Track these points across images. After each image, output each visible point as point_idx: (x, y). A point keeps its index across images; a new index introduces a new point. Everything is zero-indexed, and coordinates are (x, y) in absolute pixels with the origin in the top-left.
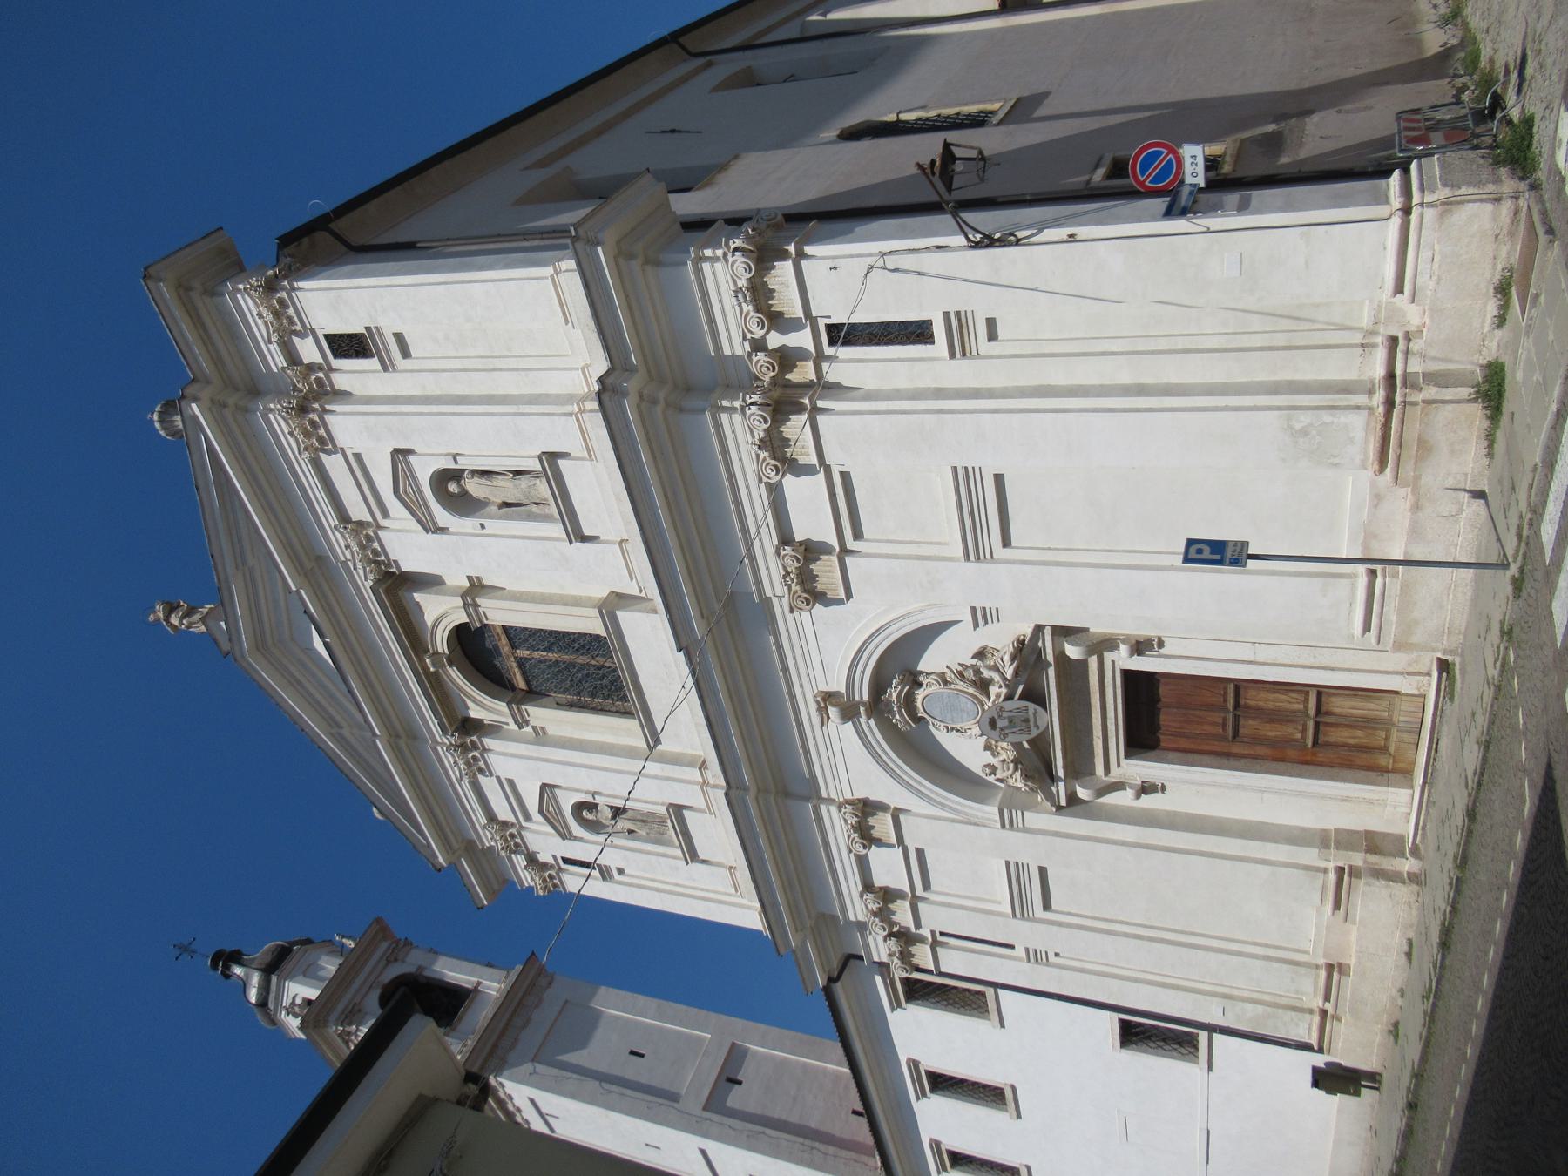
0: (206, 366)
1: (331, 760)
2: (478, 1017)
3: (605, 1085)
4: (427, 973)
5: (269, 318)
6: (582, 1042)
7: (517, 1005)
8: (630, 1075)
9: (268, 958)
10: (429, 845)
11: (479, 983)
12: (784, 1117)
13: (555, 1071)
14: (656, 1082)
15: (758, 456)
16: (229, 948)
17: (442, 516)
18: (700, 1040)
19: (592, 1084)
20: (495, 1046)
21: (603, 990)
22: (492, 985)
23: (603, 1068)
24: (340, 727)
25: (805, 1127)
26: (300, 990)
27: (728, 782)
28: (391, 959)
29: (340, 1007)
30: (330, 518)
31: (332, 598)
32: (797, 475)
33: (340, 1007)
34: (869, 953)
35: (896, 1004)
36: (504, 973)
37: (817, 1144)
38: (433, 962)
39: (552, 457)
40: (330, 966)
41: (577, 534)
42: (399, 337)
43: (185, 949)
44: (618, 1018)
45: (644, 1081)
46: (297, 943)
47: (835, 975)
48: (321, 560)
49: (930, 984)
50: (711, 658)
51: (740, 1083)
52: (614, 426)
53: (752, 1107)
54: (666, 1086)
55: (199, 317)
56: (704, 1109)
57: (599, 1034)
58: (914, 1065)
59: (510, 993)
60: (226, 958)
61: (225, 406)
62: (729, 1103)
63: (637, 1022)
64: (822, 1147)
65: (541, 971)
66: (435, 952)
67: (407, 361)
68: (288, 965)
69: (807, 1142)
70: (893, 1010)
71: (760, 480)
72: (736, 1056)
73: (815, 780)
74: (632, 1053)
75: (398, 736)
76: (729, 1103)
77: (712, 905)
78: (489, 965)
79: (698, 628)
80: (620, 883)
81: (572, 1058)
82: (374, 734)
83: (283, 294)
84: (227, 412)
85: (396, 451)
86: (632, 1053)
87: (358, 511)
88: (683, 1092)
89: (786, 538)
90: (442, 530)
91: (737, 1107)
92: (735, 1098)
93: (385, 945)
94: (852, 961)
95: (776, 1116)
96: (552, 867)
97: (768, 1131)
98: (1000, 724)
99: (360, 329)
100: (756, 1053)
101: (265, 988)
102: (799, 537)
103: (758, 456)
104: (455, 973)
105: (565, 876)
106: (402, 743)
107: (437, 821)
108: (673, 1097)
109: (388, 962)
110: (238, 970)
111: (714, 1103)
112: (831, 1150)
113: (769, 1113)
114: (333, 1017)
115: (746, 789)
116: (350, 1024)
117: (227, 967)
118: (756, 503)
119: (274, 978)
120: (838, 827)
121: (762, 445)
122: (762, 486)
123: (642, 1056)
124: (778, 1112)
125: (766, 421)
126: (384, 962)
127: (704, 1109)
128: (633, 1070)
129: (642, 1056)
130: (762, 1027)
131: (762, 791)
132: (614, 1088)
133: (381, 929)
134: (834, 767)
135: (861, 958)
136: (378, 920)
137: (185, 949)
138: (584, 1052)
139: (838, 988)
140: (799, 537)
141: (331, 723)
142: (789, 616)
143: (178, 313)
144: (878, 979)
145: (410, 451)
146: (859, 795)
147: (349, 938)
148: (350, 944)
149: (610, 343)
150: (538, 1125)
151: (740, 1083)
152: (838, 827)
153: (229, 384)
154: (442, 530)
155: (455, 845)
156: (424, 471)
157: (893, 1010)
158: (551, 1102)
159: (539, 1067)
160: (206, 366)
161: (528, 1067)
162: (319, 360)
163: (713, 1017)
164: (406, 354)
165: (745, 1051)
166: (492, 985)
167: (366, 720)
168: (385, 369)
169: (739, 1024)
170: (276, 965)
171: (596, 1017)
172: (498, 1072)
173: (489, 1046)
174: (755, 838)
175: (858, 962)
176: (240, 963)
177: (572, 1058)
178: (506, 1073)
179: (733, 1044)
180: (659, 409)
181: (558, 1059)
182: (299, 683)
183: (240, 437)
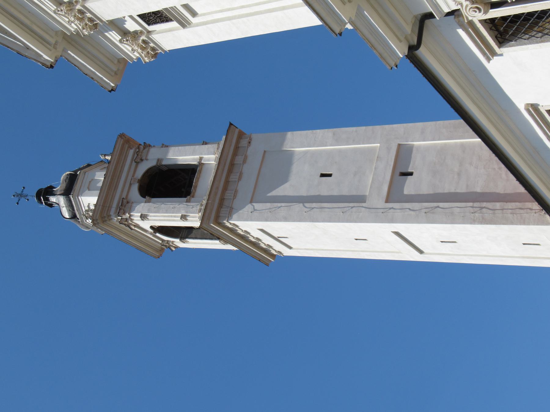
2: (204, 183)
3: (307, 205)
4: (164, 163)
5: (140, 51)
6: (284, 178)
7: (229, 165)
8: (325, 192)
9: (64, 185)
10: (28, 48)
11: (201, 159)
12: (453, 190)
13: (268, 205)
14: (345, 192)
16: (44, 186)
18: (373, 150)
19: (298, 207)
20: (222, 200)
21: (289, 134)
22: (207, 156)
23: (303, 193)
25: (419, 195)
26: (89, 201)
28: (138, 160)
29: (115, 205)
31: (392, 10)
33: (115, 205)
34: (436, 6)
35: (491, 53)
36: (216, 146)
37: (484, 204)
38: (167, 153)
40: (100, 176)
43: (20, 195)
44: (306, 152)
45: (335, 193)
46: (80, 169)
47: (415, 42)
49: (517, 17)
51: (411, 174)
53: (425, 190)
54: (354, 193)
56: (387, 201)
57: (295, 168)
58: (534, 108)
59: (220, 160)
60: (45, 193)
62: (406, 192)
63: (320, 152)
64: (490, 205)
65: (241, 135)
66: (165, 146)
68: (77, 187)
69: (477, 204)
70: (489, 60)
72: (403, 153)
74: (323, 175)
76: (406, 192)
77: (279, 14)
78: (205, 143)
80: (198, 25)
81: (279, 192)
83: (143, 37)
86: (323, 175)
88: (367, 194)
91: (413, 192)
92: (410, 186)
93: (131, 152)
94: (428, 22)
95: (446, 191)
96: (141, 32)
97: (441, 205)
100: (419, 147)
101: (70, 205)
104: (183, 156)
105: (155, 37)
107: (22, 23)
108: (360, 199)
109: (137, 163)
110: (53, 199)
111: (394, 195)
112: (498, 205)
113: (440, 191)
114: (112, 212)
116: (124, 214)
117: (47, 200)
119: (71, 196)
123: (330, 175)
124: (448, 188)
126: (134, 164)
127: (387, 201)
128: (326, 188)
129: (330, 175)
130: (420, 125)
132: (314, 205)
133: (125, 141)
135: (430, 16)
136: (122, 136)
137: (20, 195)
138: (287, 185)
139: (423, 53)
144: (461, 32)
147: (108, 155)
148: (109, 158)
150: (287, 252)
151: (411, 174)
155: (52, 41)
157: (489, 60)
158: (277, 228)
159: (257, 206)
161: (249, 207)
162: (138, 28)
163: (378, 128)
164: (194, 14)
165: (411, 148)
166: (207, 156)
168: (183, 26)
169: (400, 128)
170: (70, 188)
171: (291, 154)
172: (229, 217)
173: (217, 201)
175: (432, 20)
176: (53, 194)
177: (279, 192)
178: (235, 216)
179: (399, 145)
181: (268, 194)
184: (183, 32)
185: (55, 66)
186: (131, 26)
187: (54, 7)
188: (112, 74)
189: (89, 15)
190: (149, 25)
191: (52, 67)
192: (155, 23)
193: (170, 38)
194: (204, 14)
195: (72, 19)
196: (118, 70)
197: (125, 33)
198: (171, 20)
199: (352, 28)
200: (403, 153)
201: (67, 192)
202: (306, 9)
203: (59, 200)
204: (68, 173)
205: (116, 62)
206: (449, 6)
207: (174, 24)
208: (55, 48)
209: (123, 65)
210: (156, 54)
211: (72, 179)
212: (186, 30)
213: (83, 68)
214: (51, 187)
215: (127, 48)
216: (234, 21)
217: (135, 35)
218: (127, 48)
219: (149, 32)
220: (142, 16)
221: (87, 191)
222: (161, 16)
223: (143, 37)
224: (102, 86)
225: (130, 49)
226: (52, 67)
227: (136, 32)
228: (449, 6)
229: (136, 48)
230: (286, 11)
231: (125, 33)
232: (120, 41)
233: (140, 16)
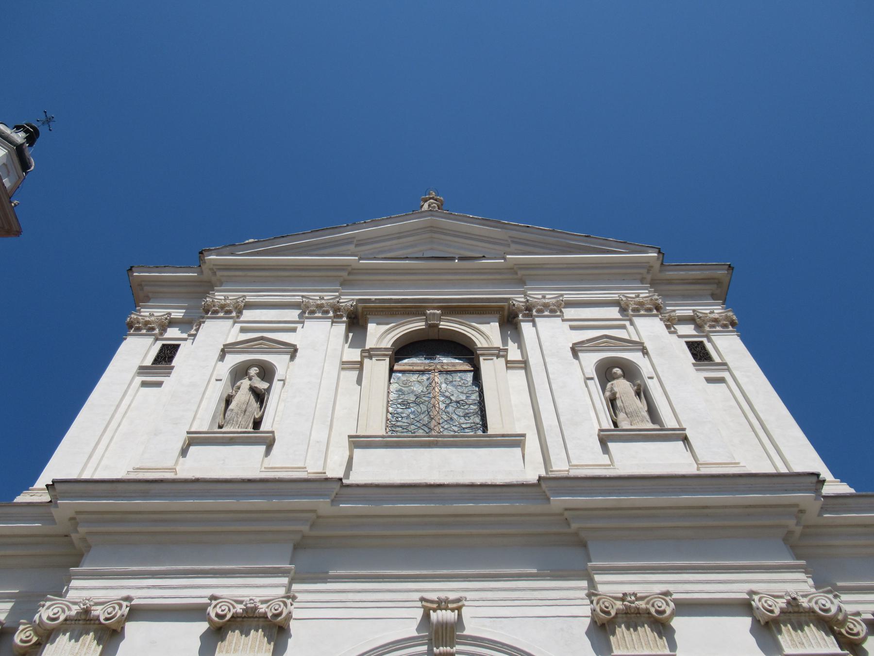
0: (671, 274)
1: (335, 229)
5: (147, 319)
10: (232, 254)
15: (241, 602)
16: (38, 141)
17: (233, 360)
24: (357, 245)
27: (348, 486)
30: (251, 298)
32: (203, 637)
39: (269, 443)
41: (194, 440)
42: (159, 384)
43: (48, 121)
48: (344, 283)
50: (519, 506)
52: (498, 490)
55: (699, 284)
60: (32, 137)
61: (648, 272)
67: (140, 383)
71: (213, 598)
73: (324, 580)
75: (349, 274)
82: (360, 259)
83: (157, 331)
84: (644, 271)
85: (296, 350)
87: (247, 315)
89: (137, 613)
90: (222, 358)
96: (161, 334)
99: (174, 363)
102: (131, 628)
103: (241, 602)
105: (151, 340)
106: (344, 274)
115: (335, 501)
117: (26, 131)
118: (733, 586)
120: (261, 591)
121: (793, 602)
122: (207, 601)
125: (107, 619)
131: (316, 520)
134: (343, 605)
136: (18, 233)
140: (131, 628)
141: (348, 241)
142: (417, 596)
143: (707, 274)
145: (293, 358)
146: (293, 624)
149: (841, 501)
152: (261, 591)
153: (345, 280)
154: (222, 358)
155: (219, 273)
156: (279, 361)
160: (671, 274)
162: (166, 336)
164: (144, 384)
167: (375, 258)
168: (141, 368)
174: (261, 496)
180: (305, 528)
182: (399, 238)
183: (629, 271)
184: (136, 363)
185: (198, 255)
186: (173, 333)
187: (248, 299)
188: (142, 283)
189: (221, 314)
190: (164, 345)
191: (201, 253)
192: (161, 350)
193: (136, 351)
194: (138, 391)
195: (228, 302)
196: (142, 290)
197: (172, 323)
198: (153, 364)
199: (15, 501)
200: (592, 379)
201: (19, 150)
202: (74, 476)
203: (19, 137)
204: (32, 168)
205: (150, 295)
206: (76, 589)
207: (149, 362)
208: (211, 269)
209: (140, 295)
210: (131, 327)
211: (25, 165)
212: (135, 369)
213: (173, 269)
214: (31, 145)
215: (159, 313)
216: (113, 408)
217: (163, 329)
218: (159, 313)
219: (157, 339)
220: (176, 347)
221: (5, 161)
222: (164, 360)
223: (157, 331)
224: (144, 267)
225: (156, 314)
226: (201, 253)
227: (165, 331)
228: (76, 589)
229: (153, 318)
230: (87, 456)
231: (172, 323)
232: (170, 314)
233: (178, 346)
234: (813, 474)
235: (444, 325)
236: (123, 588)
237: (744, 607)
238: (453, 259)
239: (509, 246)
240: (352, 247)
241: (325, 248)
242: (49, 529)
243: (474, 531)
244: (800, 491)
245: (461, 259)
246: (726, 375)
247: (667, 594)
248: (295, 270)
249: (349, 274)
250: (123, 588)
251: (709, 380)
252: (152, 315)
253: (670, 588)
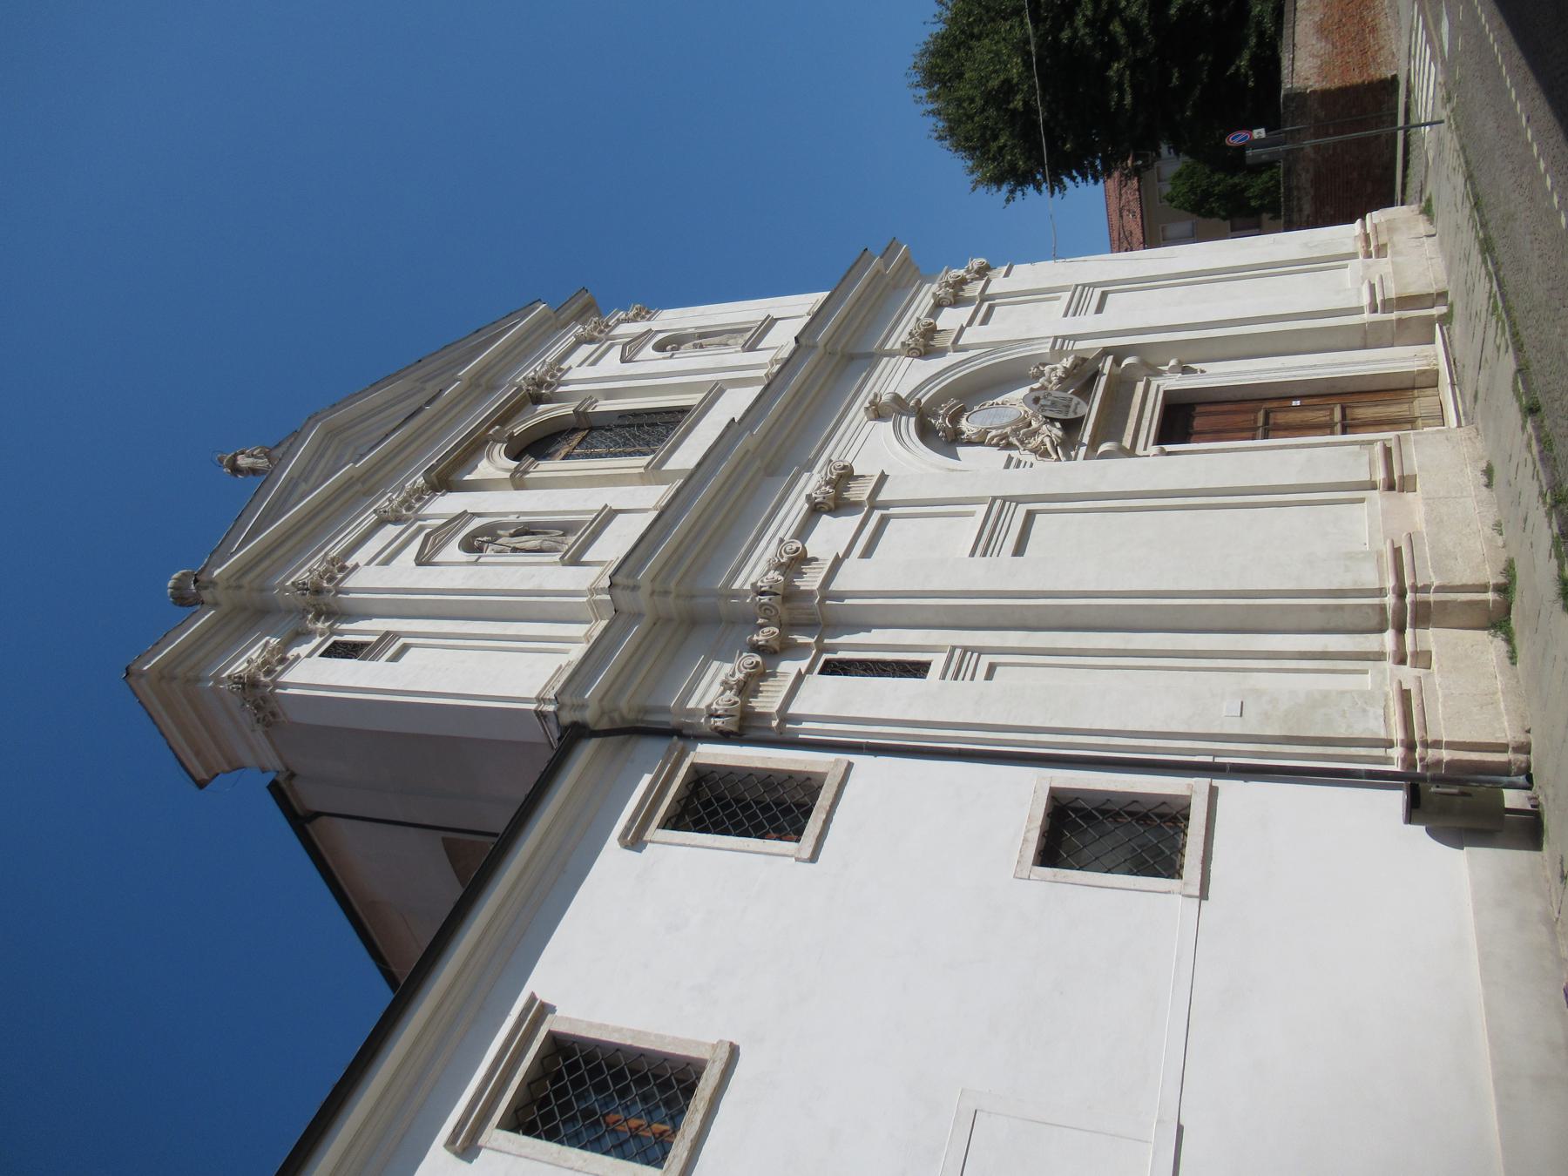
48: (369, 493)
75: (363, 483)
79: (746, 442)
98: (1042, 402)
106: (358, 487)
141: (292, 484)
155: (245, 581)
174: (723, 458)
234: (728, 426)
235: (517, 431)
236: (759, 559)
237: (816, 510)
238: (419, 410)
239: (423, 389)
240: (303, 487)
241: (290, 494)
242: (647, 621)
243: (813, 393)
244: (658, 546)
245: (429, 403)
246: (402, 641)
247: (782, 540)
248: (310, 520)
249: (363, 483)
250: (759, 559)
251: (395, 658)
252: (249, 662)
253: (780, 534)
